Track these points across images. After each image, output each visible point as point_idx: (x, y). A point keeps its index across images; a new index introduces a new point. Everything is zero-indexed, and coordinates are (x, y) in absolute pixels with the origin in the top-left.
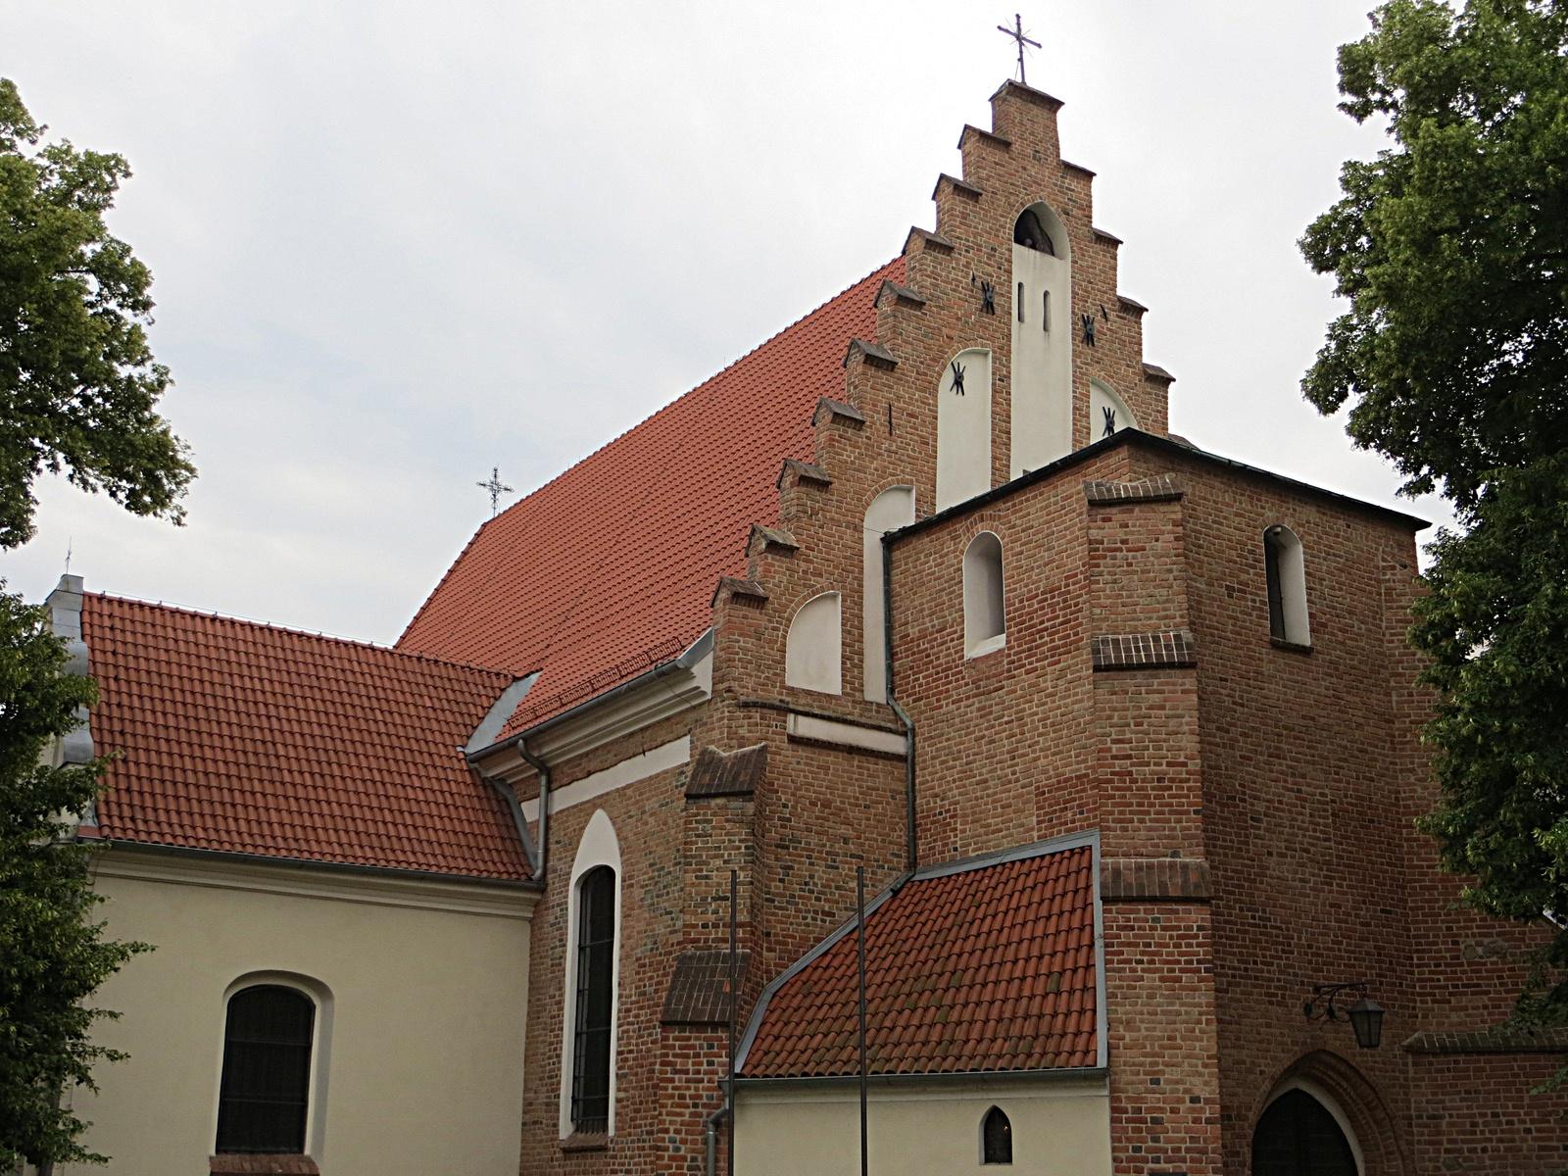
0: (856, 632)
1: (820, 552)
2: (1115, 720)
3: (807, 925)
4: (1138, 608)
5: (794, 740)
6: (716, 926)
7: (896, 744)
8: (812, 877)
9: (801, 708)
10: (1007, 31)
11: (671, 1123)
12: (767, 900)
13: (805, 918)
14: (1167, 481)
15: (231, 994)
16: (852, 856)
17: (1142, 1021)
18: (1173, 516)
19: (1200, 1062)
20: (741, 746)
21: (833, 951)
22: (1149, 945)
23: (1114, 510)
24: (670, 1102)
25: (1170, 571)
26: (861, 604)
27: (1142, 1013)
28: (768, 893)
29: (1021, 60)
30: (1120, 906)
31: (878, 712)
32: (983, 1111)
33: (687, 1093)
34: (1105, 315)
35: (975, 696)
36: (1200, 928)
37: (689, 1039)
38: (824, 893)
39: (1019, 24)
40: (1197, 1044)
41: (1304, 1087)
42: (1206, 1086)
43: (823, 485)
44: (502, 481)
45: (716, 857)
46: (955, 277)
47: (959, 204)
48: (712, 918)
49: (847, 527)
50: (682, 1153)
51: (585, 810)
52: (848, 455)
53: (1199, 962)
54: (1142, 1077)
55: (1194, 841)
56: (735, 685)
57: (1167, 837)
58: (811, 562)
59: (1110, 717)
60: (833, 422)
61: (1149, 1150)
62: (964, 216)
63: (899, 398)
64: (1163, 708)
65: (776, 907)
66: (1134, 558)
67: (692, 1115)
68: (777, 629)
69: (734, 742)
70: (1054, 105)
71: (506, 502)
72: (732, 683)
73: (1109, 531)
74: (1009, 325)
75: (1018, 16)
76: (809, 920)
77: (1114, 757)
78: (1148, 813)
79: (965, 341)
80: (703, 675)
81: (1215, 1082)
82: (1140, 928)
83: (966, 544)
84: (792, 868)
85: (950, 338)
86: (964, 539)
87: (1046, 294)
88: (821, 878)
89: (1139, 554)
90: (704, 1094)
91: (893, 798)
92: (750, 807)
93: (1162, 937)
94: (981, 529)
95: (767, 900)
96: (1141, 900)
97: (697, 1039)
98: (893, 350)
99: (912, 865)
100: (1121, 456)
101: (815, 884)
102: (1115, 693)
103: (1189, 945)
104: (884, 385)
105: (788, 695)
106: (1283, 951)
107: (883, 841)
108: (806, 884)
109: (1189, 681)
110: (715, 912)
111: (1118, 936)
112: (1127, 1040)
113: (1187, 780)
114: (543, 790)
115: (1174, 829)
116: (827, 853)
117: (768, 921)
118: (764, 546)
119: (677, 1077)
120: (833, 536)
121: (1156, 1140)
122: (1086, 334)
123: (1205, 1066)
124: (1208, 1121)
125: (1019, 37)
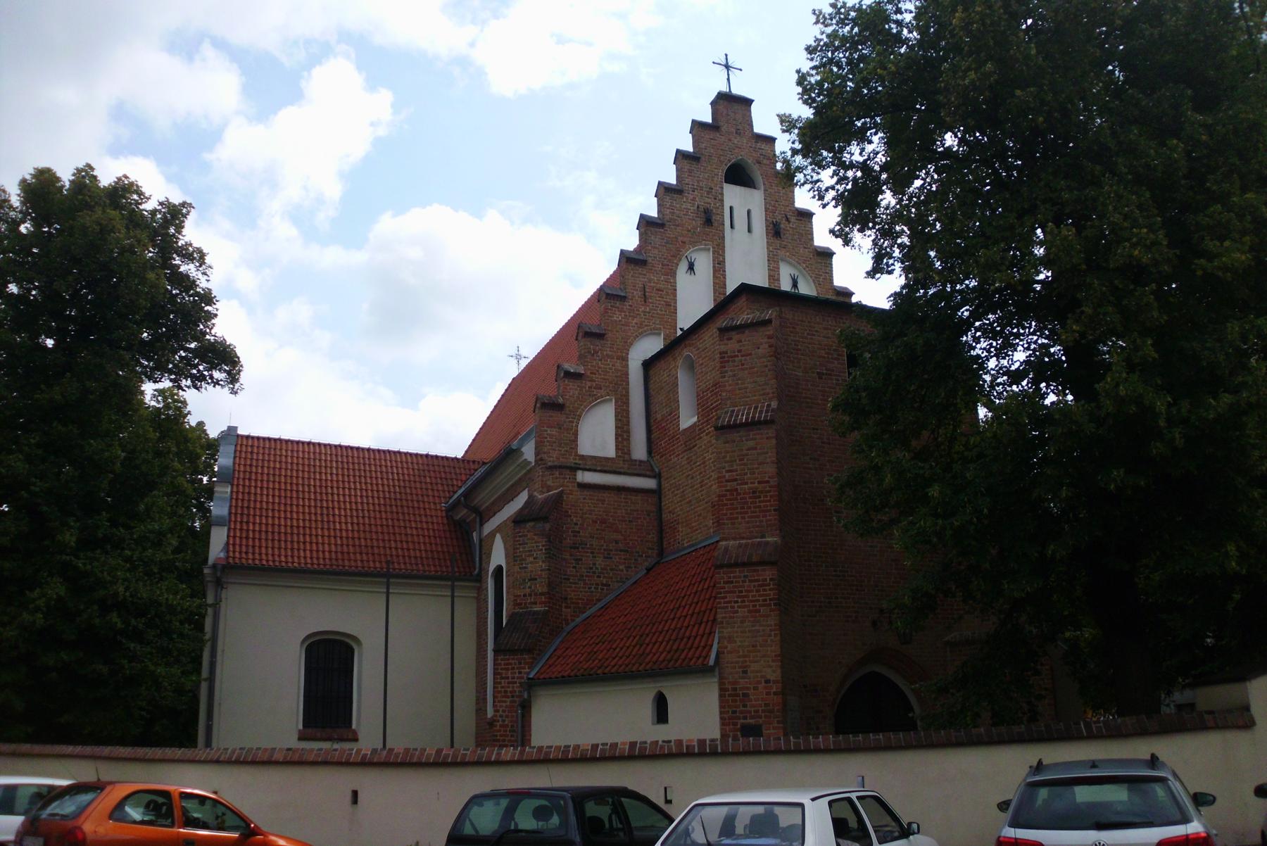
2: (728, 459)
3: (592, 592)
7: (650, 483)
8: (594, 564)
9: (588, 467)
10: (720, 64)
12: (565, 579)
13: (589, 588)
14: (769, 314)
16: (621, 551)
17: (737, 637)
18: (768, 333)
19: (770, 660)
20: (549, 491)
22: (741, 592)
23: (734, 333)
24: (499, 695)
25: (766, 366)
27: (737, 632)
28: (565, 575)
29: (728, 79)
30: (725, 569)
31: (640, 465)
32: (656, 691)
34: (787, 220)
35: (685, 451)
36: (771, 580)
37: (508, 660)
38: (603, 573)
39: (727, 59)
40: (769, 648)
41: (884, 671)
42: (774, 673)
43: (601, 336)
44: (514, 352)
46: (687, 205)
47: (686, 165)
48: (528, 591)
50: (506, 723)
51: (492, 535)
52: (617, 317)
53: (770, 600)
54: (737, 670)
55: (774, 528)
56: (545, 456)
57: (758, 526)
58: (595, 381)
59: (725, 457)
60: (606, 298)
61: (741, 712)
62: (690, 171)
64: (756, 449)
65: (571, 583)
66: (745, 360)
67: (511, 702)
69: (545, 490)
71: (524, 363)
72: (543, 455)
73: (732, 346)
75: (726, 55)
76: (593, 589)
77: (727, 481)
78: (746, 513)
79: (694, 244)
80: (529, 452)
81: (779, 671)
82: (736, 582)
83: (680, 362)
85: (683, 242)
87: (749, 212)
88: (600, 564)
89: (748, 358)
90: (517, 690)
91: (648, 515)
92: (548, 526)
93: (749, 586)
94: (686, 353)
95: (565, 579)
96: (736, 565)
97: (513, 659)
99: (661, 553)
100: (742, 301)
101: (597, 568)
102: (728, 442)
103: (765, 590)
105: (579, 460)
106: (857, 590)
107: (642, 541)
108: (591, 568)
109: (771, 432)
110: (530, 587)
112: (729, 649)
113: (770, 491)
114: (478, 526)
115: (762, 521)
116: (605, 550)
117: (566, 591)
121: (745, 706)
122: (775, 231)
123: (773, 661)
124: (775, 694)
125: (727, 67)
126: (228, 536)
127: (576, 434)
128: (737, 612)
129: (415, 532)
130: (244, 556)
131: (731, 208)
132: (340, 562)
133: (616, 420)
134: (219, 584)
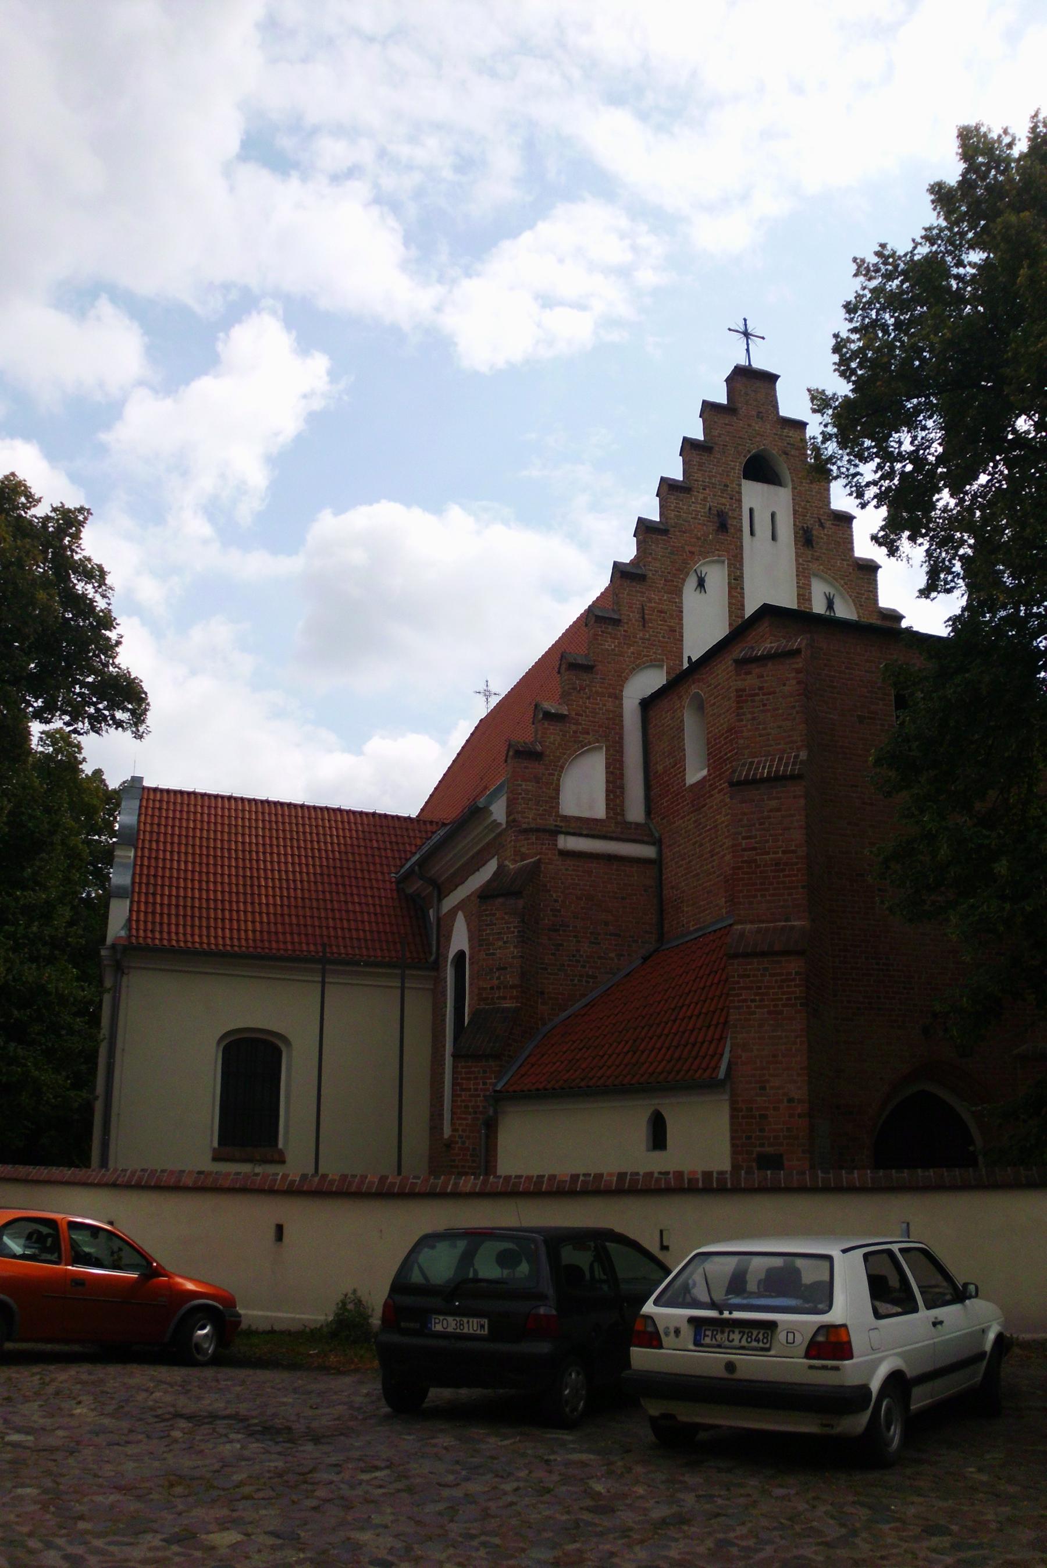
0: (618, 772)
1: (587, 716)
2: (745, 822)
4: (770, 737)
5: (566, 854)
6: (499, 988)
7: (648, 851)
8: (578, 951)
11: (460, 1125)
12: (542, 969)
14: (798, 642)
15: (221, 1048)
18: (796, 666)
21: (592, 1004)
22: (760, 988)
24: (459, 1111)
25: (794, 707)
26: (622, 752)
28: (542, 964)
33: (470, 1104)
43: (588, 669)
44: (482, 687)
45: (499, 939)
48: (496, 982)
49: (609, 697)
51: (453, 913)
52: (609, 645)
53: (796, 998)
58: (581, 724)
63: (650, 601)
64: (779, 810)
66: (768, 700)
68: (553, 775)
69: (518, 858)
70: (773, 378)
71: (494, 701)
74: (741, 539)
76: (576, 982)
77: (744, 850)
79: (704, 554)
80: (499, 811)
82: (754, 976)
83: (686, 702)
84: (561, 945)
85: (692, 553)
86: (685, 697)
87: (773, 515)
94: (694, 689)
98: (644, 566)
100: (764, 627)
101: (581, 956)
103: (788, 986)
104: (637, 591)
105: (561, 821)
108: (574, 956)
110: (498, 978)
111: (738, 983)
113: (797, 864)
118: (541, 716)
119: (463, 1093)
120: (598, 704)
121: (762, 1130)
122: (805, 539)
124: (799, 1116)
126: (131, 911)
127: (557, 790)
128: (754, 1013)
129: (358, 908)
130: (149, 935)
131: (751, 510)
132: (267, 944)
133: (607, 773)
134: (119, 969)
